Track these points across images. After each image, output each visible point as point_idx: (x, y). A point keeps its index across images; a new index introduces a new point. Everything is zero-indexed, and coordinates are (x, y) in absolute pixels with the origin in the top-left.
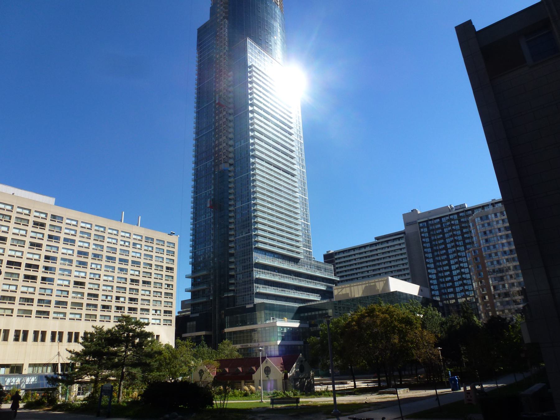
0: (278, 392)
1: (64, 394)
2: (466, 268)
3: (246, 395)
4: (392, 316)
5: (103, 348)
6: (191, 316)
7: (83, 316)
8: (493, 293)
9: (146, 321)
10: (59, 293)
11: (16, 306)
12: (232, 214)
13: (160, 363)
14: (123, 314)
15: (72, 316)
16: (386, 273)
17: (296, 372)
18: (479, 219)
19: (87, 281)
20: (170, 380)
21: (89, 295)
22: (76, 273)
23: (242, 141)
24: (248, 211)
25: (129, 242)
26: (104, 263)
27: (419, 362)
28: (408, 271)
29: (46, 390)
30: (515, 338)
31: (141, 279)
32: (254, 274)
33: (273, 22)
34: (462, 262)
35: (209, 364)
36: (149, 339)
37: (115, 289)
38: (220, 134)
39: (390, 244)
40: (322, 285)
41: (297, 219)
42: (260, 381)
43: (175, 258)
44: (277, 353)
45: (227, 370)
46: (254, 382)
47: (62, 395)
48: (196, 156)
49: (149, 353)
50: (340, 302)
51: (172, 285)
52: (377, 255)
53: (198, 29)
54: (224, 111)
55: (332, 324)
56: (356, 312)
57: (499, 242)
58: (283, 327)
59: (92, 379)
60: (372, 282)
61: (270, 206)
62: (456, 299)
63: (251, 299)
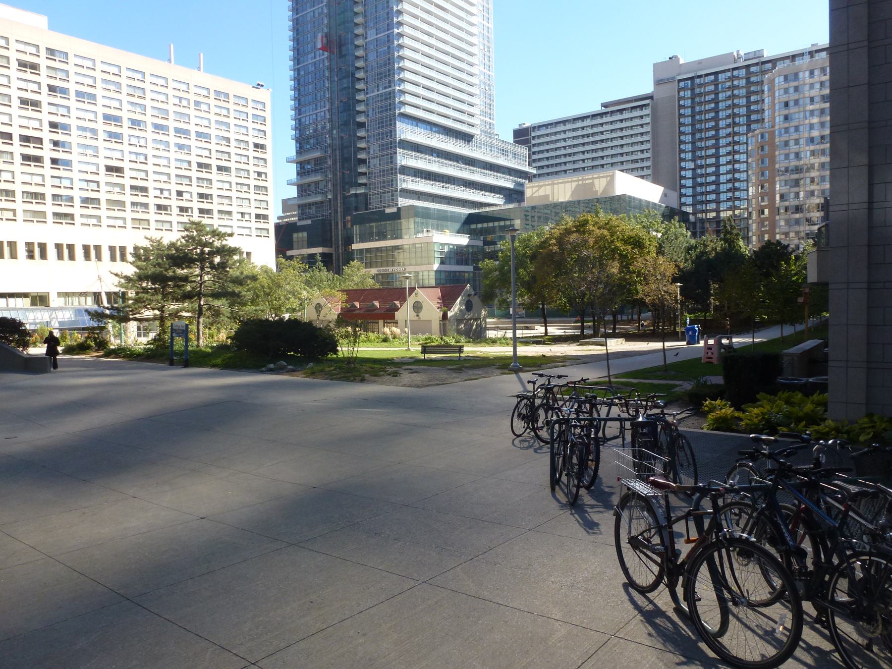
0: (433, 337)
1: (118, 336)
2: (743, 162)
3: (385, 340)
5: (166, 270)
6: (299, 224)
8: (777, 205)
9: (229, 231)
10: (84, 185)
11: (19, 205)
12: (360, 53)
13: (255, 293)
14: (192, 219)
15: (112, 222)
16: (612, 164)
17: (460, 310)
18: (782, 79)
19: (126, 165)
20: (272, 317)
21: (133, 187)
24: (389, 48)
26: (150, 134)
27: (645, 302)
28: (648, 163)
30: (795, 274)
31: (214, 163)
32: (399, 158)
34: (738, 152)
36: (236, 257)
39: (626, 115)
40: (507, 180)
44: (433, 283)
45: (357, 304)
46: (397, 323)
47: (115, 337)
49: (237, 278)
50: (534, 208)
51: (266, 174)
55: (519, 242)
57: (807, 122)
58: (442, 245)
59: (155, 315)
62: (718, 211)
63: (393, 200)
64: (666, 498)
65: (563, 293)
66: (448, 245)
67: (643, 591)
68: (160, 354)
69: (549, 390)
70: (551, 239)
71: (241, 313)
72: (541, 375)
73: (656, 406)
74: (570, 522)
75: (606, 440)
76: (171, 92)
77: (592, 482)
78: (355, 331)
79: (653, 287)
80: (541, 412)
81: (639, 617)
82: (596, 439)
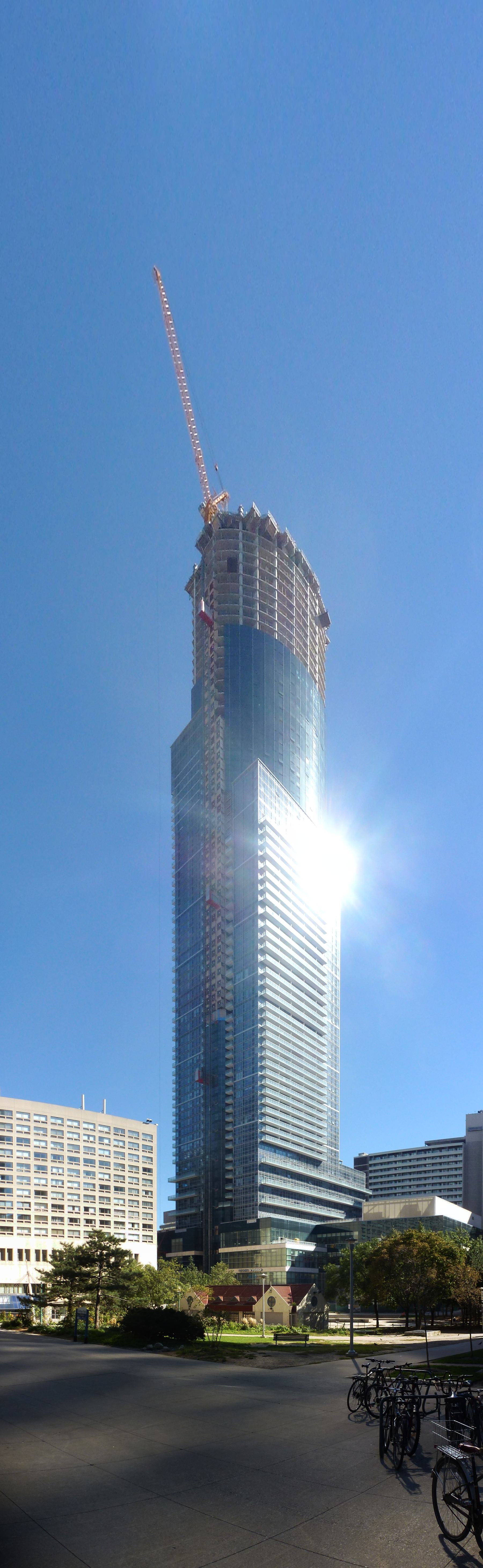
1: (39, 1317)
3: (244, 1328)
4: (432, 1246)
5: (75, 1268)
6: (176, 1232)
7: (50, 1231)
9: (122, 1237)
10: (20, 1205)
12: (229, 1092)
15: (37, 1232)
16: (433, 1191)
17: (307, 1305)
19: (49, 1189)
20: (153, 1307)
22: (36, 1181)
23: (247, 971)
25: (94, 1137)
26: (66, 1166)
28: (460, 1192)
29: (20, 1311)
31: (112, 1184)
32: (259, 1178)
33: (304, 723)
35: (200, 1290)
36: (127, 1258)
37: (82, 1199)
38: (213, 959)
39: (444, 1153)
40: (348, 1199)
41: (321, 1103)
42: (262, 1313)
43: (154, 1156)
44: (285, 1281)
45: (222, 1298)
46: (254, 1314)
47: (37, 1318)
48: (178, 1000)
49: (127, 1274)
50: (369, 1222)
52: (425, 1165)
53: (172, 747)
54: (219, 915)
56: (388, 1237)
58: (294, 1250)
60: (413, 1200)
61: (284, 1080)
64: (473, 1460)
65: (392, 1293)
66: (298, 1250)
67: (455, 1540)
68: (67, 1332)
69: (379, 1373)
70: (382, 1248)
71: (129, 1302)
72: (373, 1361)
73: (465, 1385)
74: (396, 1485)
75: (425, 1414)
76: (81, 1132)
77: (414, 1450)
78: (219, 1320)
79: (463, 1289)
80: (373, 1391)
81: (452, 1563)
82: (417, 1413)
